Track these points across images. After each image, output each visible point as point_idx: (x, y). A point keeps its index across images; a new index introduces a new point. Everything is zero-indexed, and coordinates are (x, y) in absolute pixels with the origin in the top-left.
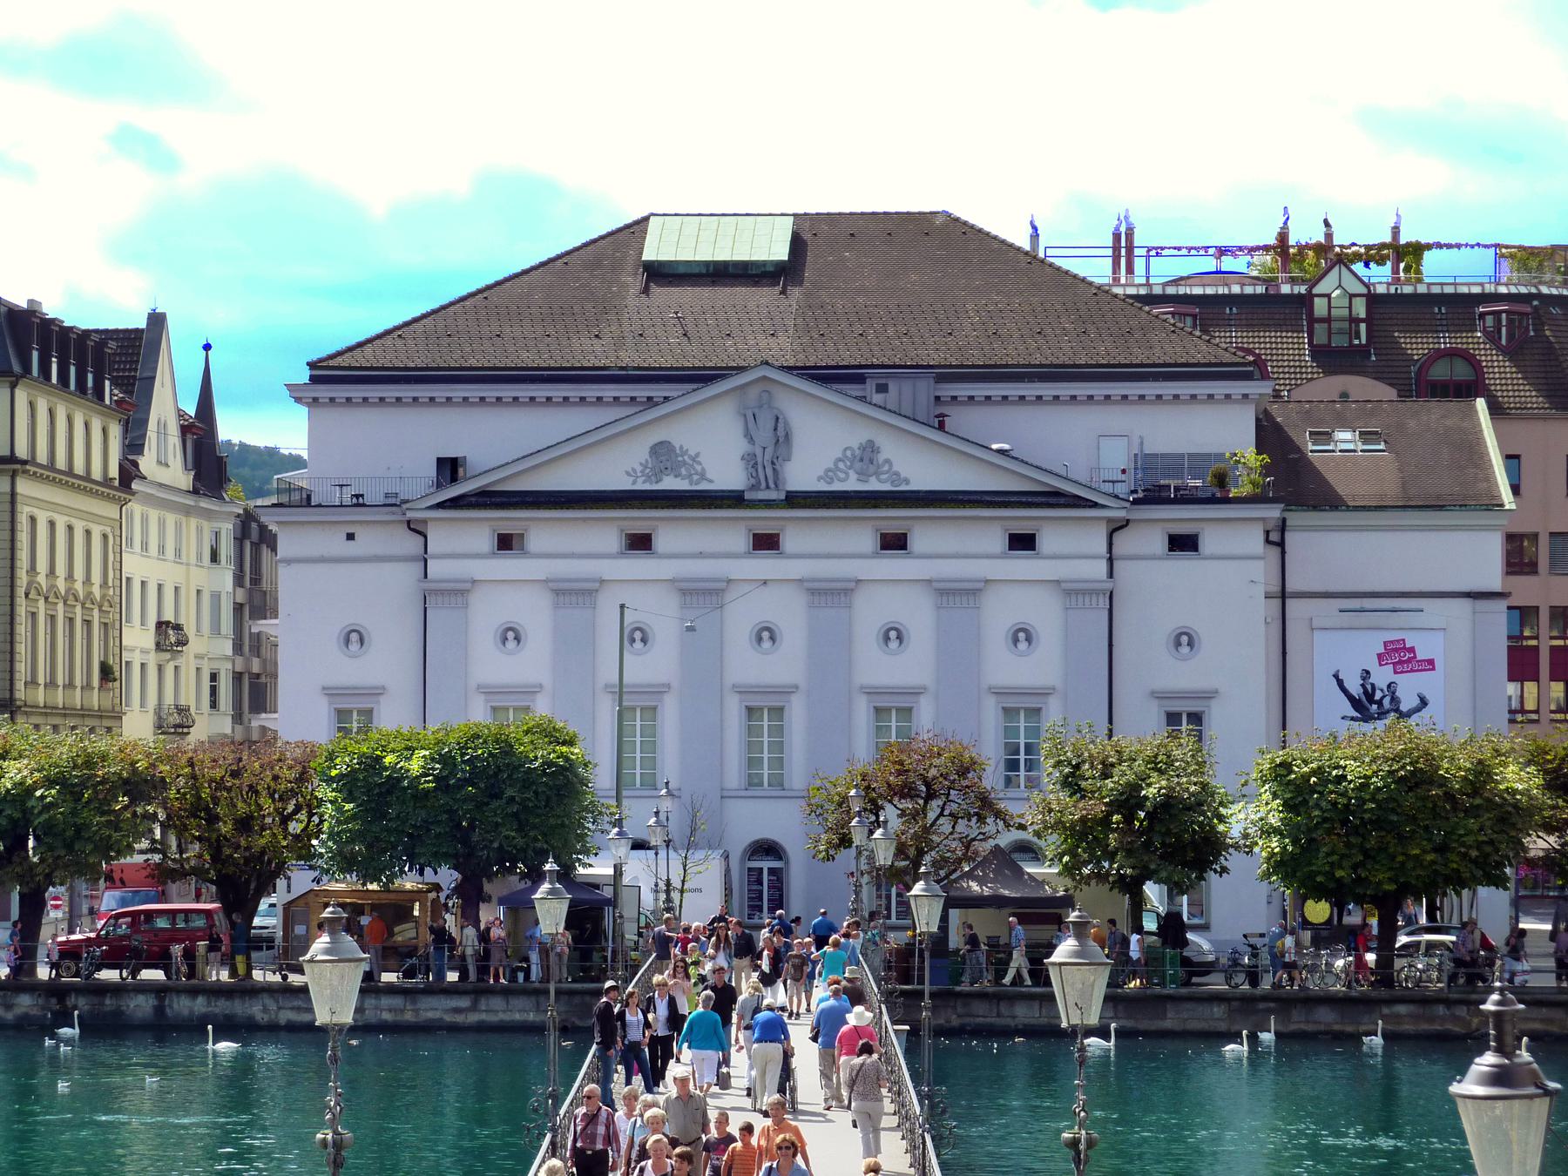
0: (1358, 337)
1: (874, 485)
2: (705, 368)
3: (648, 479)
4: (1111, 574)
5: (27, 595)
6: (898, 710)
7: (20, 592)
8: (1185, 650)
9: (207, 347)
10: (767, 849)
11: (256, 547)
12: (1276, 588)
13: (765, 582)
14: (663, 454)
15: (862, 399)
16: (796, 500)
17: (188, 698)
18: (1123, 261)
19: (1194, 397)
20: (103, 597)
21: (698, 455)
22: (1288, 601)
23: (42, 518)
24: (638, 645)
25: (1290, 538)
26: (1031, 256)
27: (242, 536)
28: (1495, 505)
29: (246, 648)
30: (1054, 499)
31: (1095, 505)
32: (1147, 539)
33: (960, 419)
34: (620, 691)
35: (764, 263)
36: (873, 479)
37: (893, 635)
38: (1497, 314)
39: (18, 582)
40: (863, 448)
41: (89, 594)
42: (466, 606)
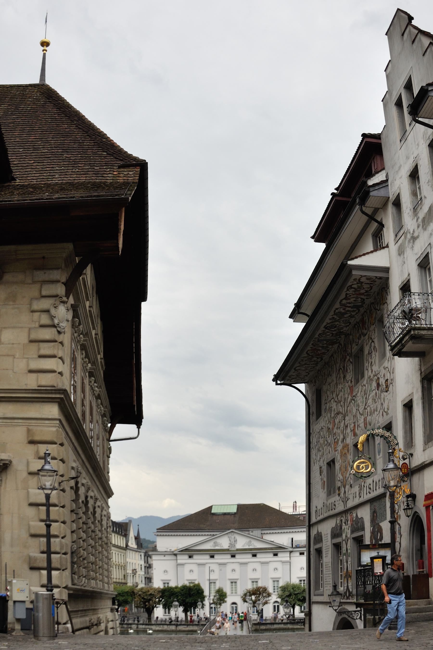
1: (251, 547)
4: (290, 559)
9: (138, 525)
10: (234, 603)
11: (147, 557)
15: (249, 534)
17: (137, 581)
26: (279, 511)
30: (281, 548)
31: (287, 549)
42: (184, 567)
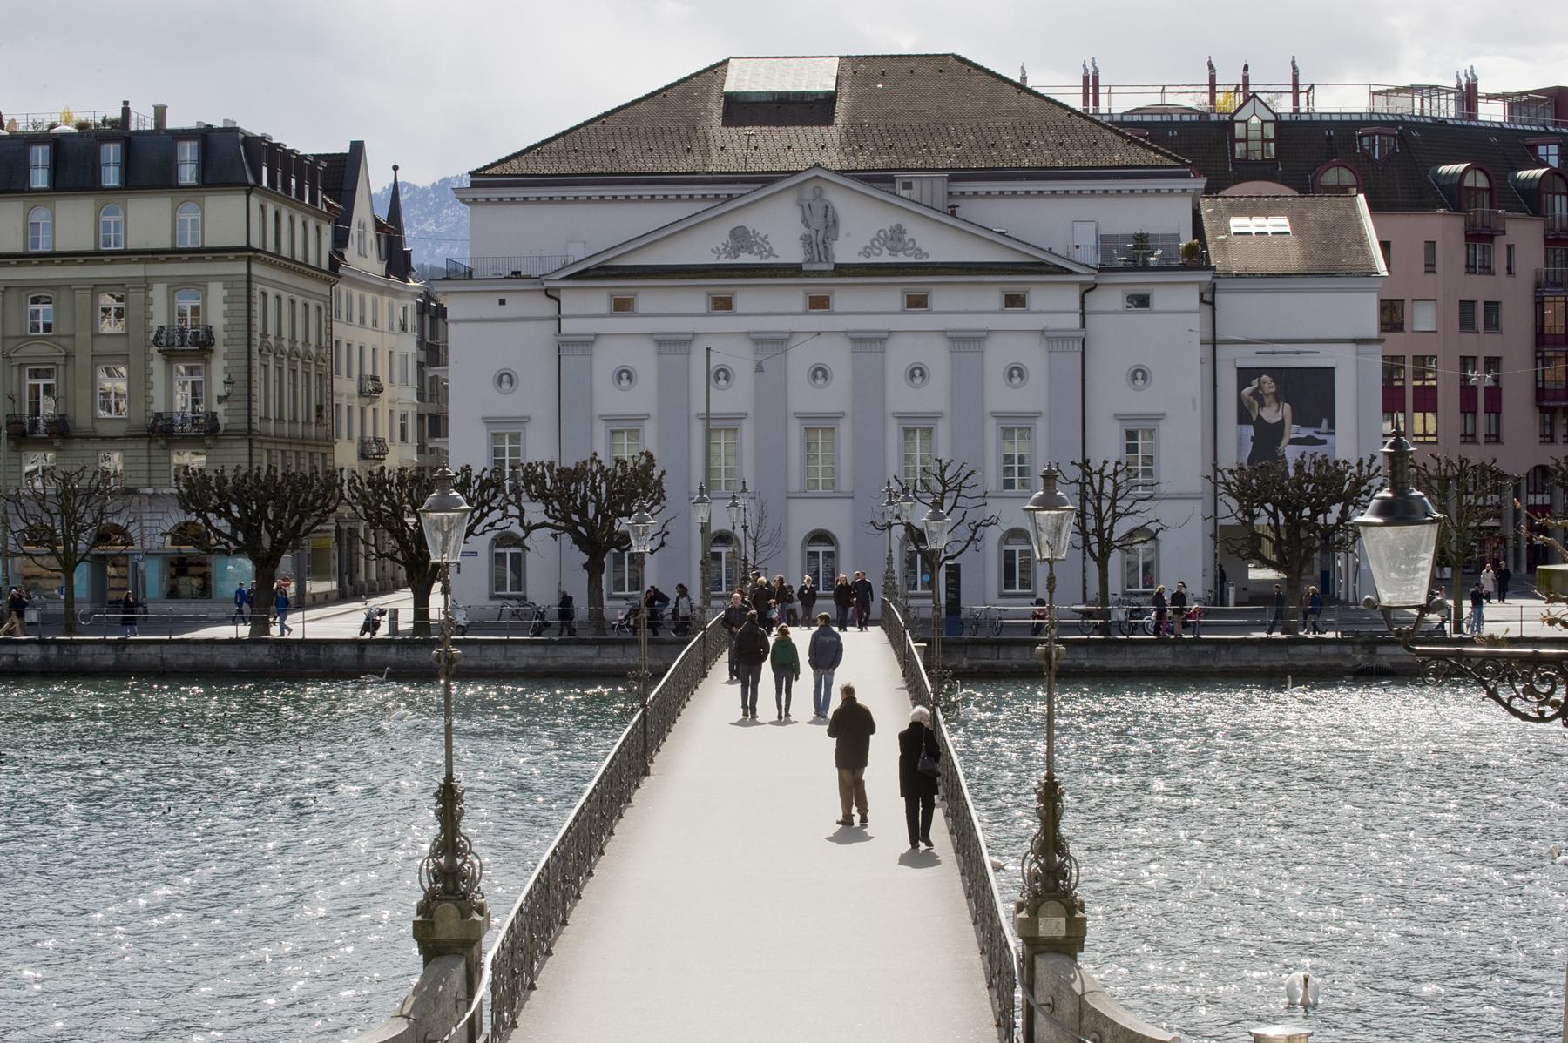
0: (1269, 152)
1: (901, 258)
2: (771, 172)
3: (728, 255)
4: (1083, 325)
5: (260, 351)
6: (922, 430)
7: (255, 349)
8: (1140, 383)
9: (395, 168)
10: (821, 537)
12: (1209, 337)
13: (819, 334)
14: (740, 238)
16: (842, 270)
17: (383, 433)
18: (1091, 97)
19: (1145, 191)
20: (318, 355)
21: (766, 236)
22: (1218, 347)
23: (271, 293)
24: (722, 383)
25: (1220, 299)
27: (423, 309)
28: (1371, 273)
29: (427, 397)
31: (1070, 272)
32: (1110, 298)
33: (968, 209)
34: (707, 417)
35: (817, 93)
36: (901, 254)
37: (917, 373)
38: (1371, 135)
39: (253, 342)
40: (892, 230)
41: (307, 352)
